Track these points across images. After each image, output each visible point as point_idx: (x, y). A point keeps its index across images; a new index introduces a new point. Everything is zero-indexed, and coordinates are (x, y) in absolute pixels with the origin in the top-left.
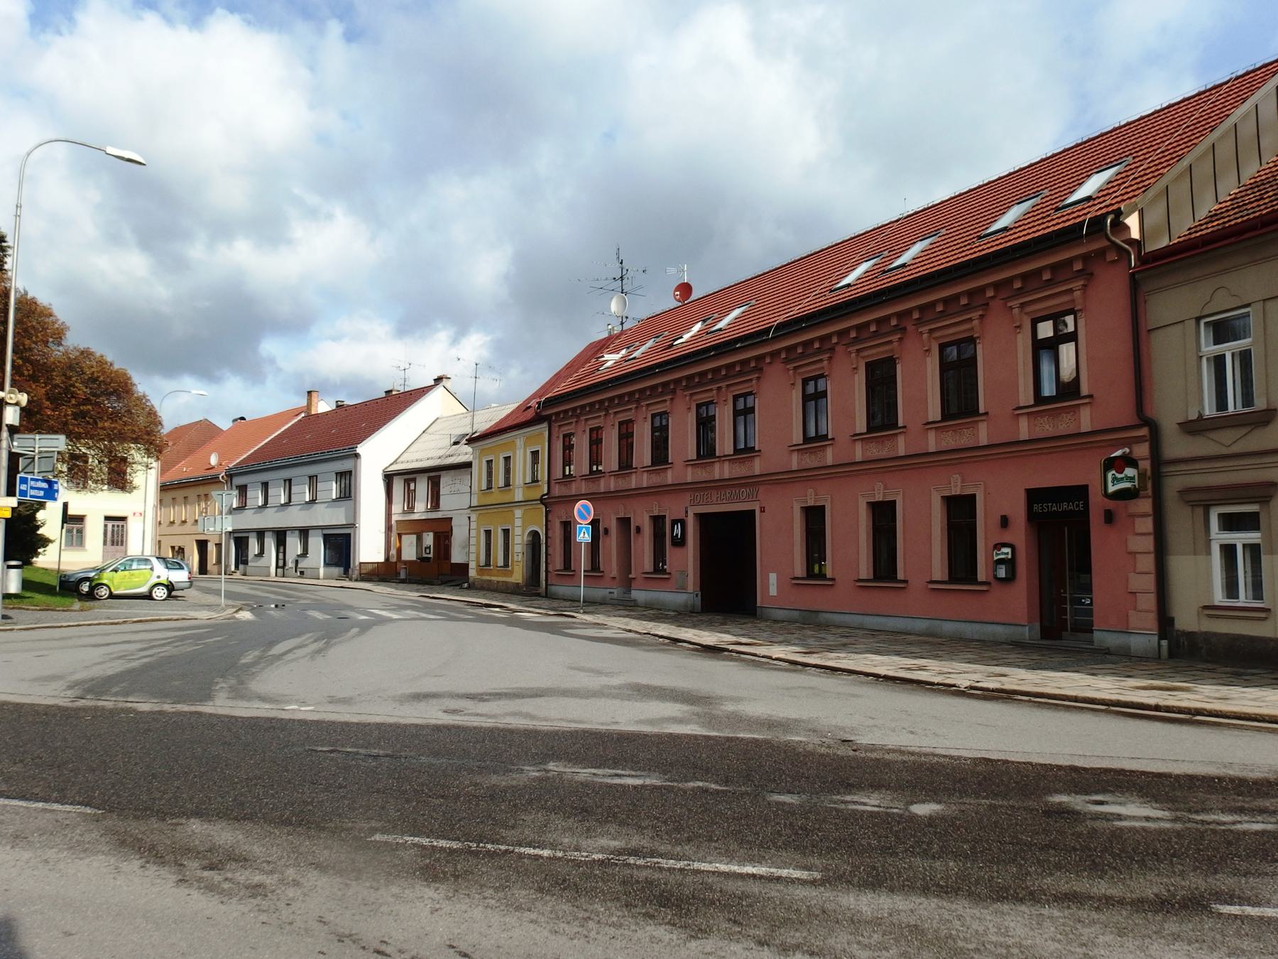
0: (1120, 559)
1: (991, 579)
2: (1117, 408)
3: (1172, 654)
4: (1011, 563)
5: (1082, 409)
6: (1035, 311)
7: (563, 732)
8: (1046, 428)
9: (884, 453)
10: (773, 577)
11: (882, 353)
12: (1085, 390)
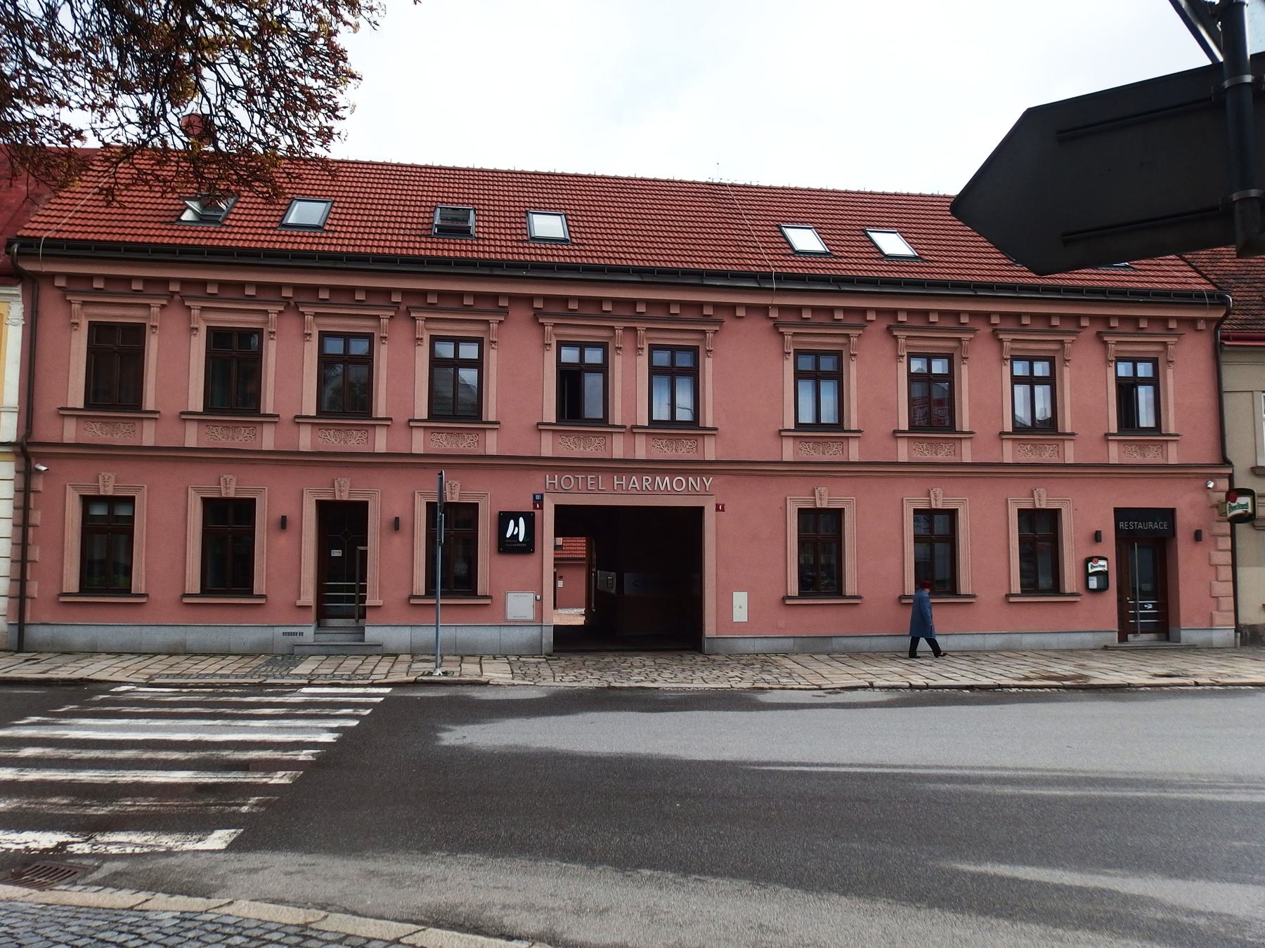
0: (1195, 570)
1: (1081, 590)
2: (1204, 452)
3: (1243, 644)
4: (1102, 575)
5: (266, 427)
6: (96, 315)
7: (1200, 877)
8: (812, 453)
9: (941, 457)
10: (740, 600)
11: (338, 326)
12: (490, 413)
